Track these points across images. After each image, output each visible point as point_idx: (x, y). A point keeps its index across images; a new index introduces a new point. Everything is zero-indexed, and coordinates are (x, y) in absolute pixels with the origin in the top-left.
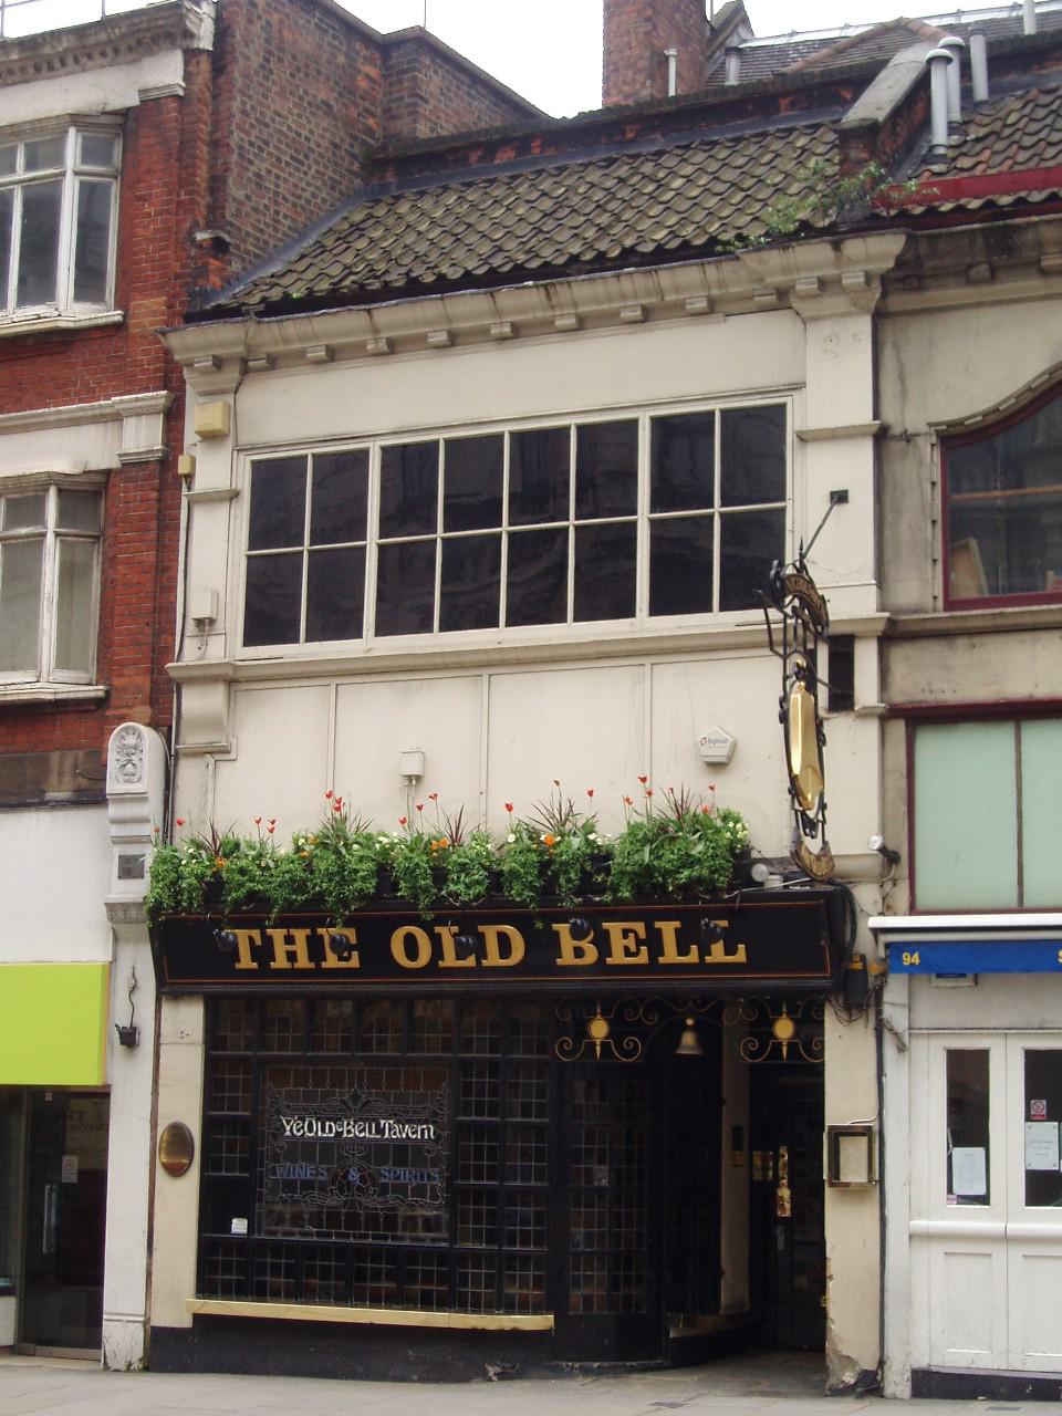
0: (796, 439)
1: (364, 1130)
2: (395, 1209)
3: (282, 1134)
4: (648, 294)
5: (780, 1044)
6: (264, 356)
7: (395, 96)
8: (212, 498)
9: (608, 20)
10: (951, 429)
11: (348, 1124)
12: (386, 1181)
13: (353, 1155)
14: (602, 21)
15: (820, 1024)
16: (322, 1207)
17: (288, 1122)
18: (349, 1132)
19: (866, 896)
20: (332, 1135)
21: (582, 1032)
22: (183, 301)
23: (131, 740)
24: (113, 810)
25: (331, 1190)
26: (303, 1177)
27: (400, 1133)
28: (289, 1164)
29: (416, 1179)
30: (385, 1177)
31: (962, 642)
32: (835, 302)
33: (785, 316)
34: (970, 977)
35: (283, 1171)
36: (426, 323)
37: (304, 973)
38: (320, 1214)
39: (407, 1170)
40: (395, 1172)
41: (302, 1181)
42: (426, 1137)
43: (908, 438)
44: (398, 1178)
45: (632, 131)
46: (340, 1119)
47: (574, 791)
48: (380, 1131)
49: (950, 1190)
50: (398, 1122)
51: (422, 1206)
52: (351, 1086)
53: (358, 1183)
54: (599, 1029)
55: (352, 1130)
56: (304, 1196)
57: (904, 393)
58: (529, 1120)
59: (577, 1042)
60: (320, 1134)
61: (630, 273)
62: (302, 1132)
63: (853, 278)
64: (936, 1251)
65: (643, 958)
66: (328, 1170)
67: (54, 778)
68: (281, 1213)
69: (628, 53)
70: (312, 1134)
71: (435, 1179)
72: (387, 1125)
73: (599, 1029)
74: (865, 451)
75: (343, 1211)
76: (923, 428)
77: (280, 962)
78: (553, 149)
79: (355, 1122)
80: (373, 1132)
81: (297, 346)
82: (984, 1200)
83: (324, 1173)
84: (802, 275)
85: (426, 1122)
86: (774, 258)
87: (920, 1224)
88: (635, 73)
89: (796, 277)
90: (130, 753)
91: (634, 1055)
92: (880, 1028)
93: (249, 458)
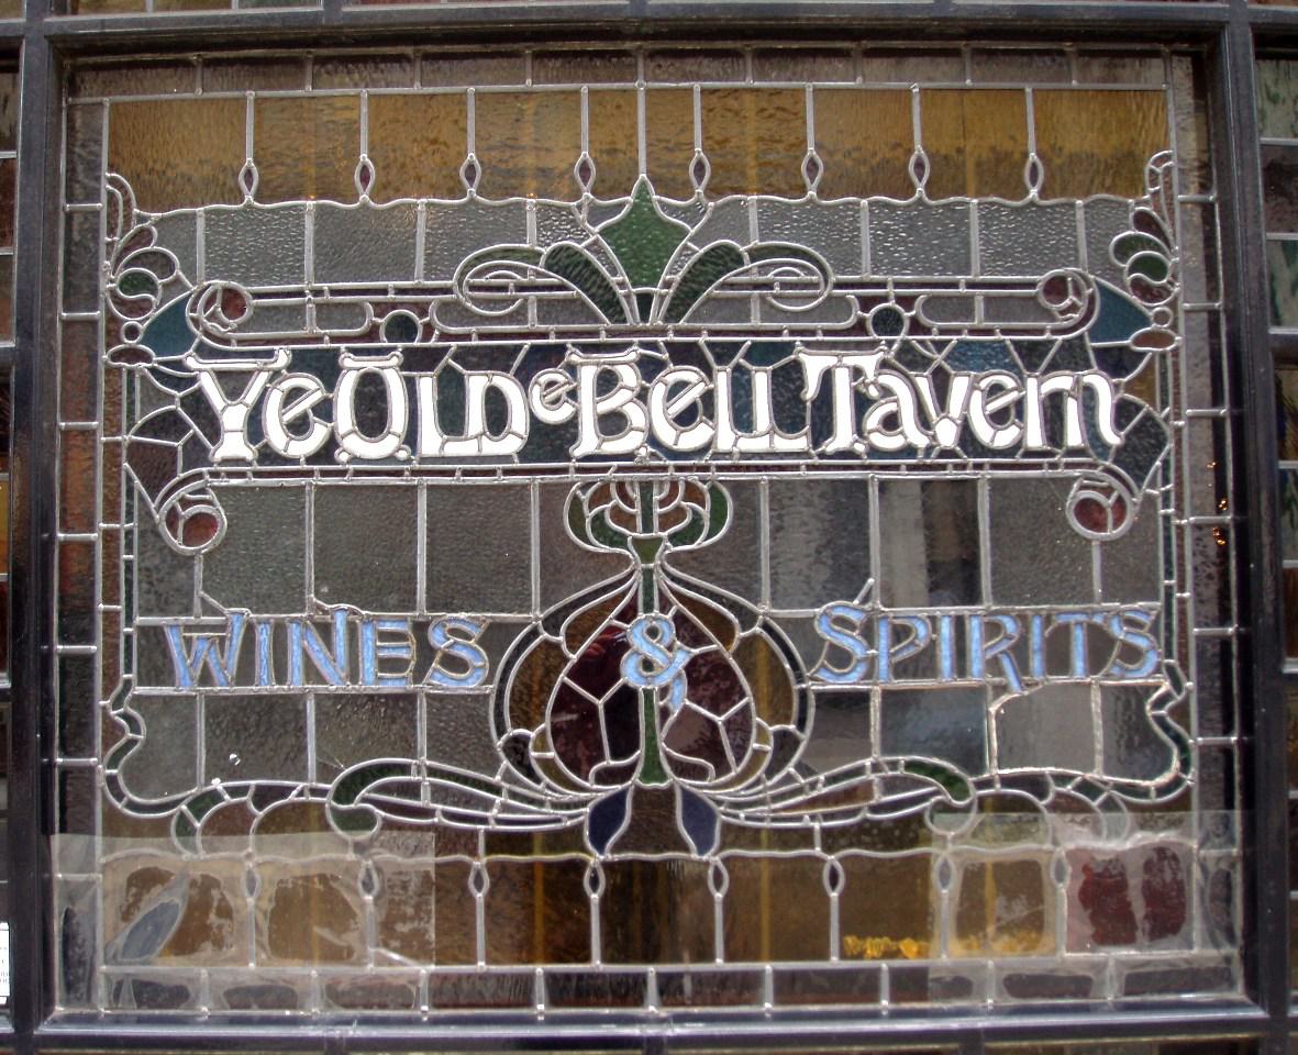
2: (909, 831)
3: (197, 454)
11: (607, 382)
12: (848, 682)
13: (647, 549)
16: (466, 841)
20: (510, 445)
25: (517, 749)
26: (337, 684)
27: (924, 422)
29: (1023, 667)
30: (841, 658)
38: (450, 883)
39: (975, 617)
40: (900, 633)
41: (217, 706)
44: (923, 663)
46: (548, 356)
50: (909, 360)
51: (1065, 805)
53: (679, 699)
56: (347, 791)
60: (431, 440)
62: (319, 434)
66: (494, 638)
68: (207, 884)
70: (387, 446)
71: (1132, 655)
75: (595, 859)
79: (649, 368)
85: (1072, 358)
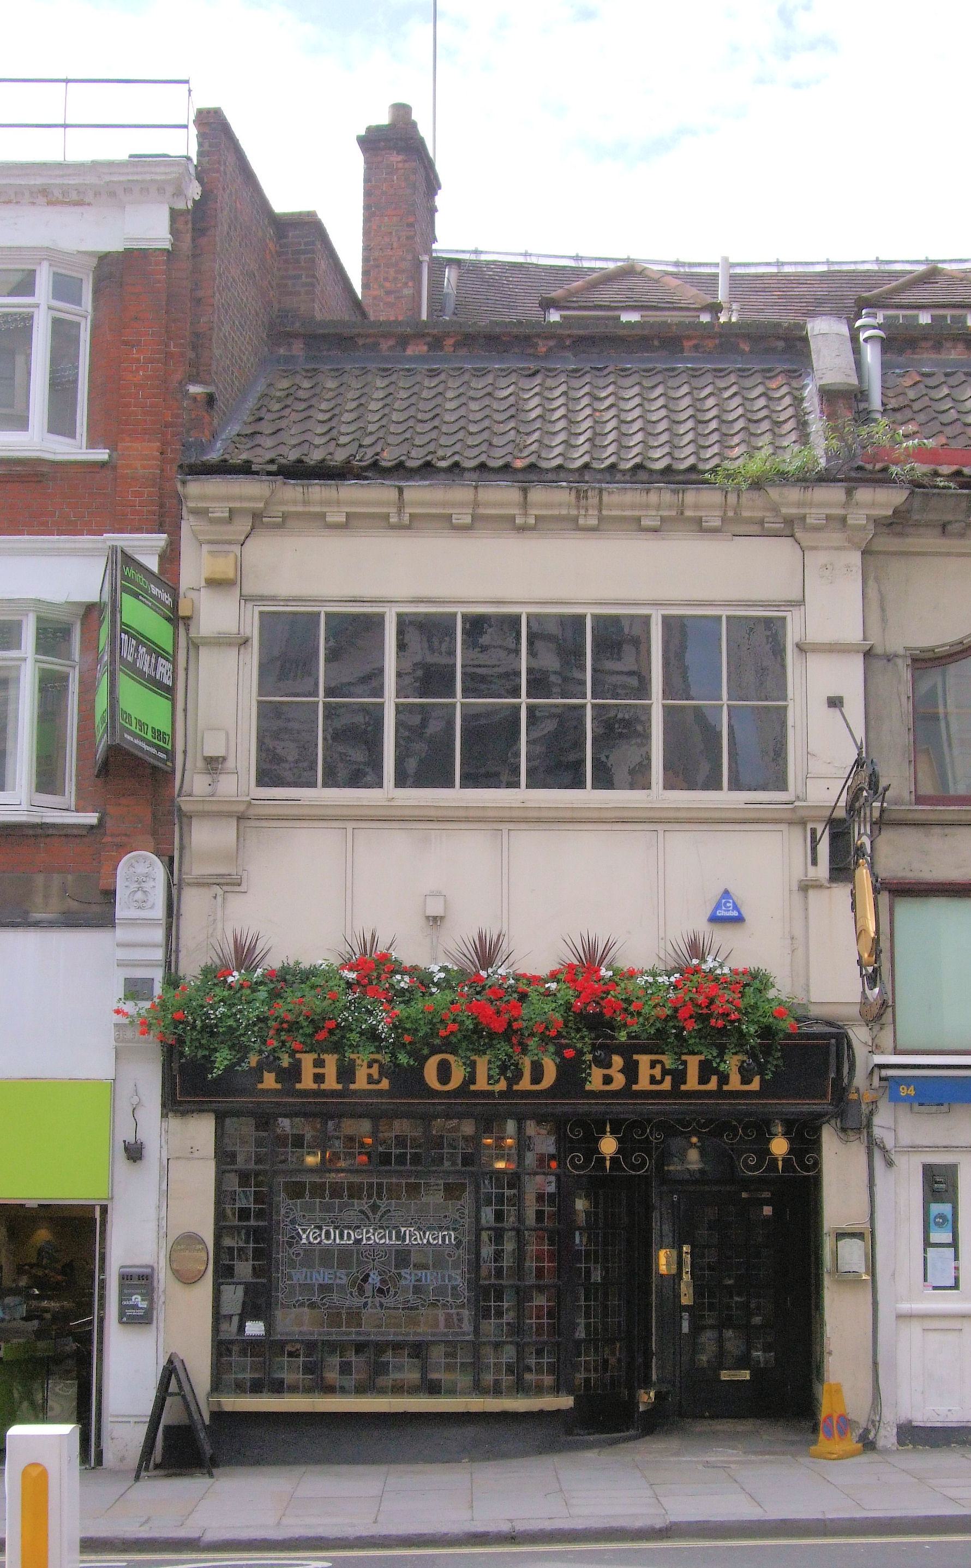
0: (796, 650)
1: (384, 1236)
3: (298, 1242)
4: (670, 507)
5: (776, 1159)
6: (280, 514)
7: (291, 273)
8: (221, 642)
9: (367, 219)
10: (923, 654)
11: (368, 1232)
14: (361, 218)
15: (816, 1145)
17: (304, 1231)
18: (368, 1239)
19: (859, 1035)
20: (351, 1242)
21: (592, 1150)
22: (176, 449)
23: (141, 869)
24: (120, 934)
27: (421, 1239)
28: (304, 1270)
31: (937, 830)
32: (837, 538)
33: (786, 544)
34: (946, 1105)
35: (299, 1276)
36: (453, 505)
37: (333, 1093)
38: (339, 1314)
42: (447, 1242)
43: (889, 658)
45: (544, 346)
46: (358, 1227)
47: (365, 923)
48: (401, 1237)
49: (925, 1280)
50: (419, 1229)
52: (369, 1197)
54: (608, 1146)
55: (372, 1237)
56: (322, 1299)
57: (884, 620)
58: (248, 1223)
59: (588, 1160)
60: (338, 1241)
61: (660, 489)
63: (858, 518)
64: (916, 1328)
65: (667, 1085)
66: (347, 1275)
67: (39, 900)
69: (389, 252)
70: (330, 1242)
72: (408, 1232)
73: (608, 1146)
74: (857, 664)
76: (901, 651)
77: (307, 1082)
78: (465, 349)
79: (375, 1230)
80: (394, 1239)
81: (317, 509)
82: (956, 1287)
83: (343, 1277)
84: (813, 511)
85: (448, 1229)
86: (794, 494)
87: (905, 1307)
88: (397, 272)
89: (807, 511)
90: (140, 882)
91: (643, 1169)
92: (872, 1146)
93: (257, 609)
